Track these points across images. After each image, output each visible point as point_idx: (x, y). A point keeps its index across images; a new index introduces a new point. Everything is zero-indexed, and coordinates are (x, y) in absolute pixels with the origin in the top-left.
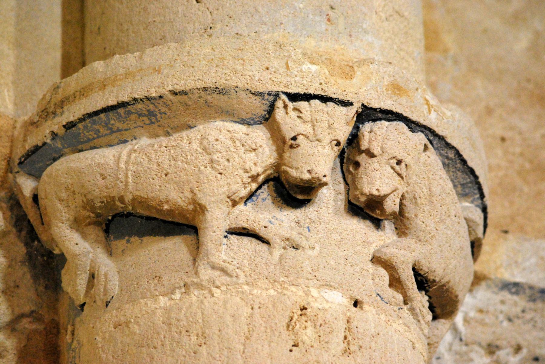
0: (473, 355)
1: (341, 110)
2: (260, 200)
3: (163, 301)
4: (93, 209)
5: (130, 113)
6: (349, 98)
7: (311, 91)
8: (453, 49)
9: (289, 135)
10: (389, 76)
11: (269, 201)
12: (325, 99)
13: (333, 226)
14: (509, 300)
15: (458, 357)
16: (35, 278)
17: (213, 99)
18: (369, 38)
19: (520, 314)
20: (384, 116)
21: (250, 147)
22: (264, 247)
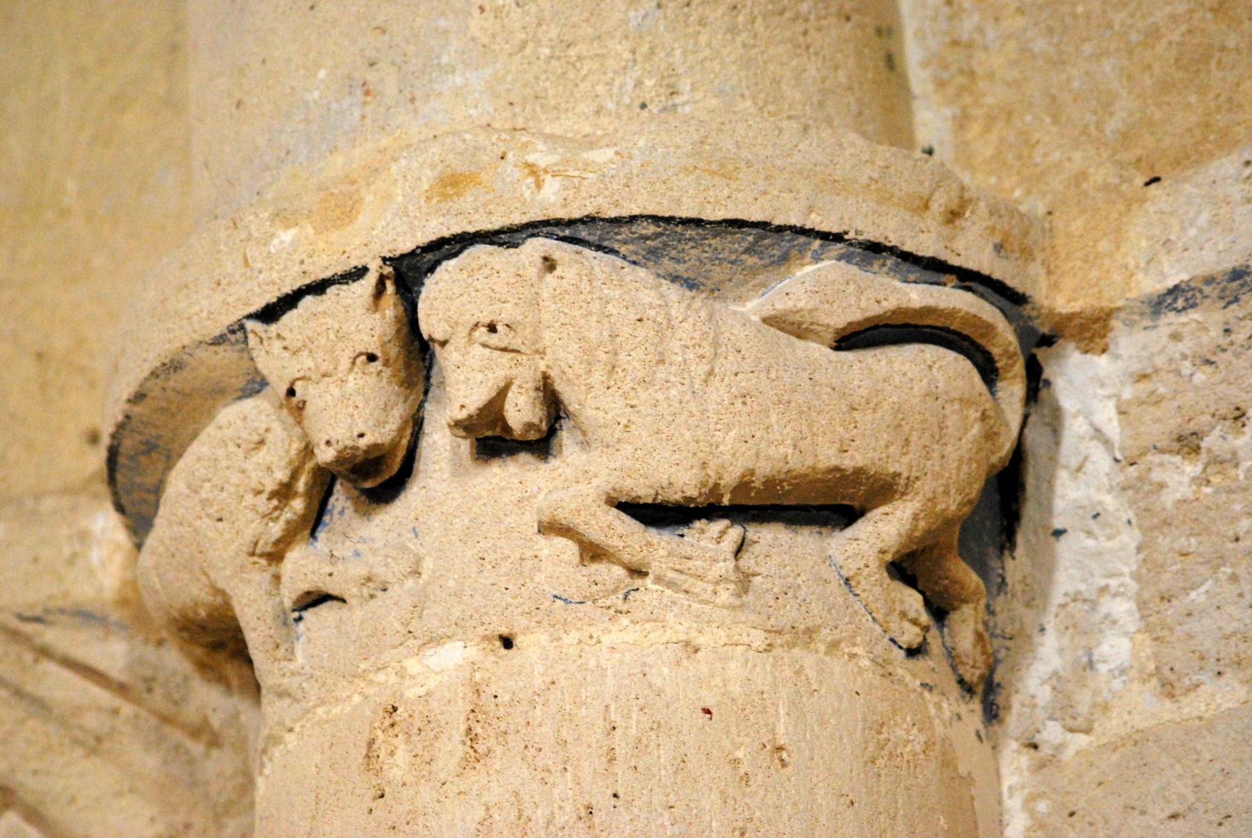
0: (1157, 475)
2: (336, 516)
6: (355, 262)
7: (287, 290)
10: (433, 166)
11: (349, 512)
12: (318, 288)
13: (455, 503)
14: (1184, 324)
15: (1130, 493)
19: (1224, 342)
20: (438, 254)
21: (250, 442)
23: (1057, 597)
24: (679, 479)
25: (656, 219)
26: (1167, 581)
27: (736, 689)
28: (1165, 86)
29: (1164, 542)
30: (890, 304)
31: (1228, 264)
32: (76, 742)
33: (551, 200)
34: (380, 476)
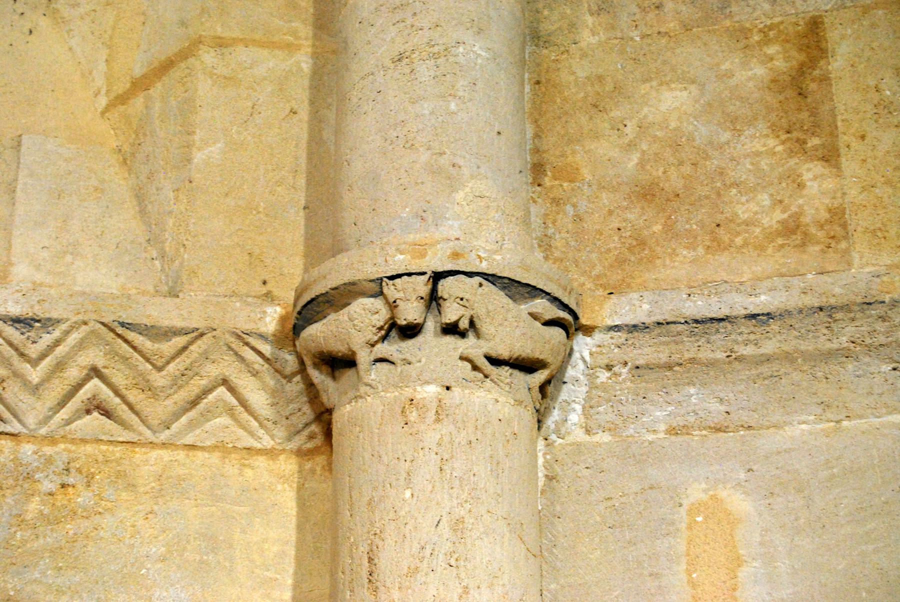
0: (598, 374)
1: (422, 277)
4: (316, 357)
5: (319, 303)
8: (588, 177)
9: (392, 300)
11: (397, 338)
17: (350, 288)
18: (450, 222)
22: (392, 367)
23: (560, 399)
24: (504, 352)
25: (510, 279)
26: (593, 403)
27: (506, 414)
28: (611, 266)
29: (594, 392)
30: (557, 316)
31: (633, 323)
32: (249, 371)
33: (484, 267)
34: (410, 331)
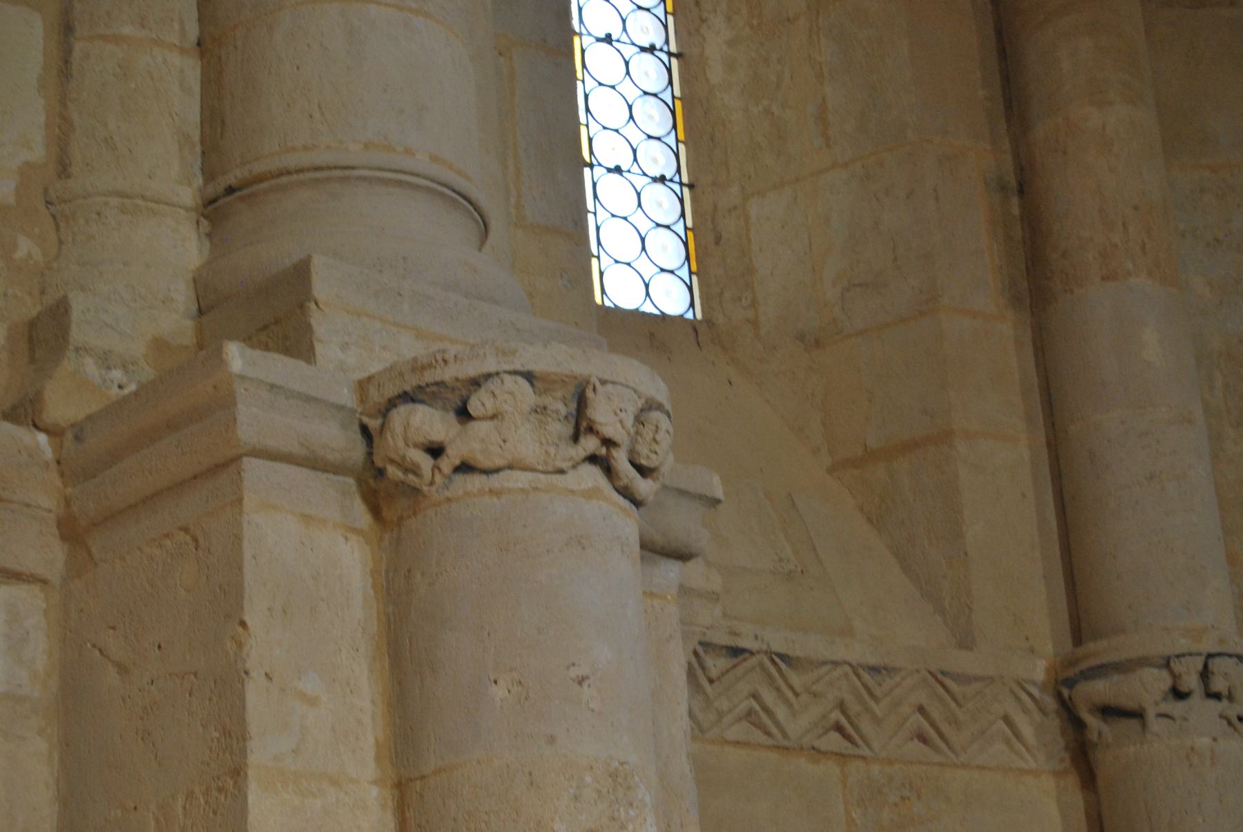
3: (1132, 749)
16: (431, 405)
